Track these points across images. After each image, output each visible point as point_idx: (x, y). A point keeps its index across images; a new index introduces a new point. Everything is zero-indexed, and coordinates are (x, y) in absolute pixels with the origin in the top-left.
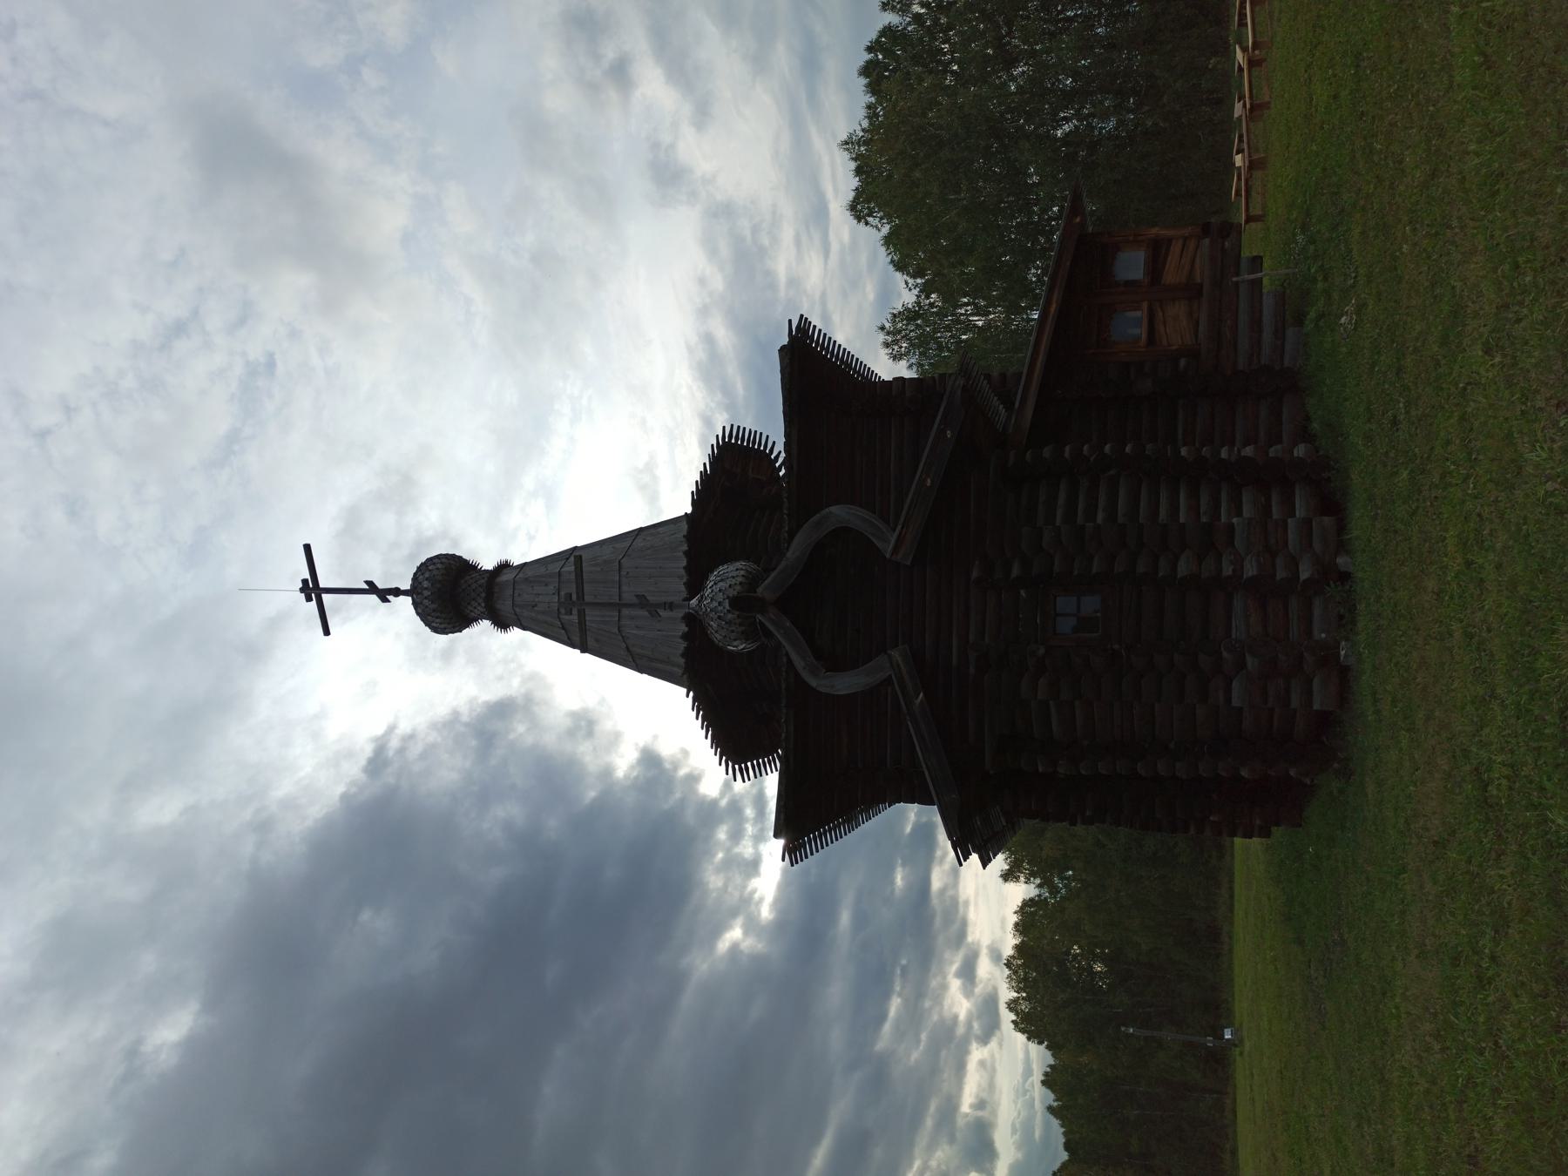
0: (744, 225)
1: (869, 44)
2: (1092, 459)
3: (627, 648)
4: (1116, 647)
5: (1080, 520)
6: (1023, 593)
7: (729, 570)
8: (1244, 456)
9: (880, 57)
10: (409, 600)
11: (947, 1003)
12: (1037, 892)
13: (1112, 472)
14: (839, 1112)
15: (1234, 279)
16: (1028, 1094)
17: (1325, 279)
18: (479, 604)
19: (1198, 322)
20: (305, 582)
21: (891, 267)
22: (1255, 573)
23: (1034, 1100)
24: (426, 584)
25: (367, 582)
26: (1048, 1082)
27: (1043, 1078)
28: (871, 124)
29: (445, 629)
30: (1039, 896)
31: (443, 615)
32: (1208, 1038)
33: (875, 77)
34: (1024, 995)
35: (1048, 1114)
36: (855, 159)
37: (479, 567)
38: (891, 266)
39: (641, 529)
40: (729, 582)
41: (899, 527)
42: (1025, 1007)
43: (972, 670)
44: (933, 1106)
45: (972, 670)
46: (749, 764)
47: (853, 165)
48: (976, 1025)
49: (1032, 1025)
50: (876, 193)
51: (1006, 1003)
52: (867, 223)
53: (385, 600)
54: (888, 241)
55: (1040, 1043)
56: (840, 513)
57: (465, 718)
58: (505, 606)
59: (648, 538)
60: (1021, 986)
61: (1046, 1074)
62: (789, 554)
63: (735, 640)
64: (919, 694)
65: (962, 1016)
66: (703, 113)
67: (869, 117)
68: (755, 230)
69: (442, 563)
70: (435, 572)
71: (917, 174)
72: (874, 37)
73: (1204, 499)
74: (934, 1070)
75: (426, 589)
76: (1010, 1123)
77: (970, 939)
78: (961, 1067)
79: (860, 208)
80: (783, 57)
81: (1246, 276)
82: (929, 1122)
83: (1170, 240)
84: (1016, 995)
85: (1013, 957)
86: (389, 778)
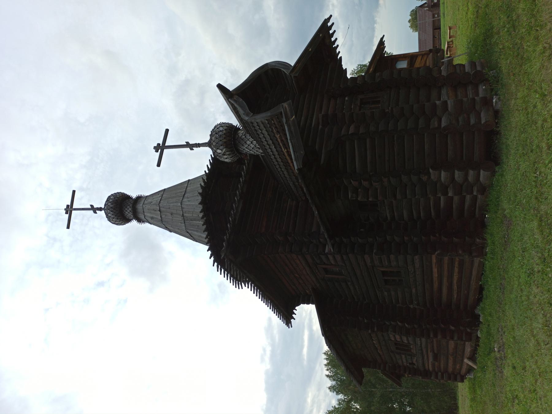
10: (103, 211)
18: (130, 207)
20: (68, 206)
31: (115, 211)
45: (320, 127)
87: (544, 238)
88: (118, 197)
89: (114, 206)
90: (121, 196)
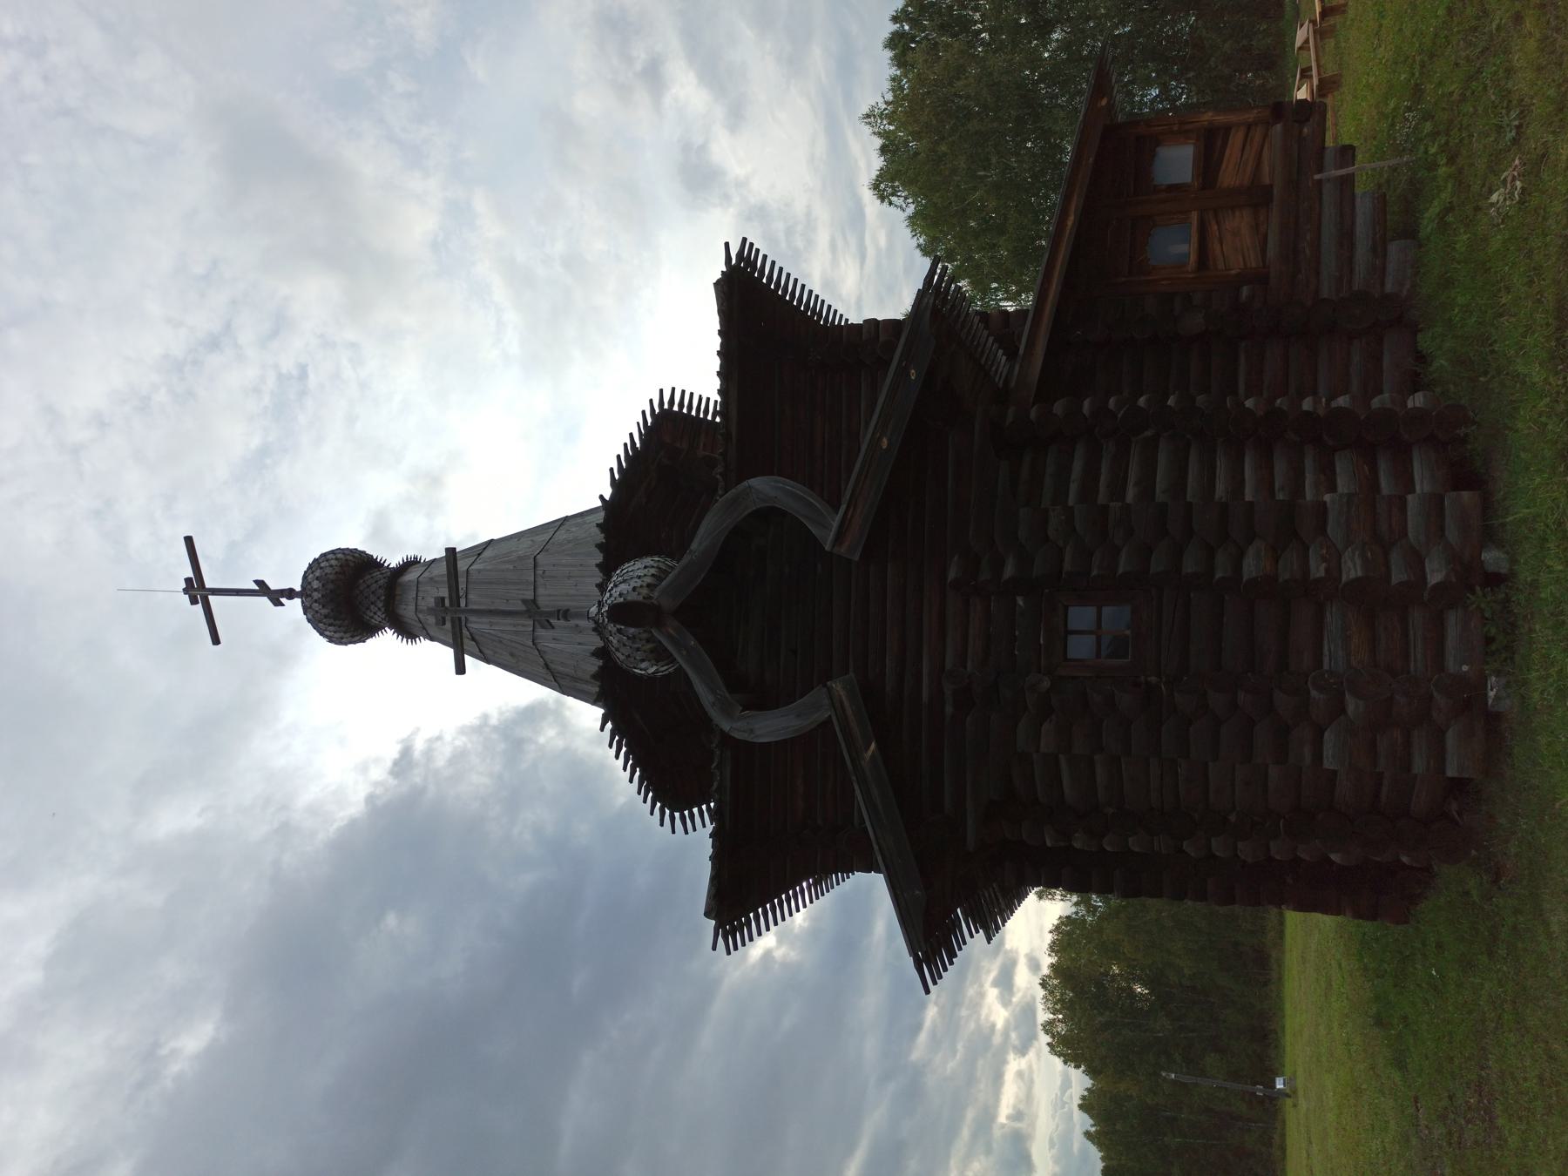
0: (779, 227)
1: (895, 14)
2: (1119, 416)
3: (546, 665)
4: (1153, 679)
5: (1102, 498)
6: (1020, 601)
7: (636, 567)
8: (1335, 408)
9: (907, 28)
10: (297, 602)
11: (984, 1012)
12: (1074, 909)
13: (1148, 433)
14: (874, 1121)
15: (1317, 177)
16: (1067, 1106)
17: (1452, 160)
18: (379, 609)
19: (1266, 237)
20: (188, 581)
21: (918, 253)
22: (1360, 574)
23: (1072, 1114)
24: (316, 584)
25: (257, 582)
26: (1085, 1106)
27: (1080, 1102)
28: (895, 96)
29: (342, 638)
30: (1077, 913)
31: (338, 622)
32: (1258, 1086)
33: (901, 49)
34: (1060, 1016)
35: (1085, 1139)
36: (879, 134)
37: (386, 565)
38: (918, 250)
39: (566, 519)
40: (633, 584)
41: (844, 507)
42: (1061, 1028)
43: (949, 709)
44: (970, 1115)
45: (949, 709)
46: (695, 810)
47: (878, 142)
48: (1013, 1035)
49: (1068, 1048)
50: (901, 171)
51: (1042, 1025)
52: (891, 203)
53: (278, 603)
54: (913, 221)
55: (1077, 1067)
56: (764, 487)
57: (494, 721)
58: (408, 612)
59: (574, 529)
60: (1058, 1007)
61: (1083, 1098)
62: (694, 546)
63: (643, 661)
64: (869, 747)
65: (1000, 1025)
66: (737, 116)
67: (893, 90)
68: (789, 232)
69: (336, 559)
70: (328, 570)
71: (943, 148)
72: (900, 7)
73: (1280, 468)
74: (971, 1080)
75: (315, 590)
76: (1048, 1137)
77: (1008, 946)
78: (998, 1078)
79: (883, 187)
80: (818, 58)
81: (1333, 172)
82: (965, 1133)
83: (1227, 129)
84: (1052, 1016)
85: (1049, 977)
86: (417, 778)
87: (1348, 1043)
88: (332, 581)
89: (332, 610)
90: (340, 573)
